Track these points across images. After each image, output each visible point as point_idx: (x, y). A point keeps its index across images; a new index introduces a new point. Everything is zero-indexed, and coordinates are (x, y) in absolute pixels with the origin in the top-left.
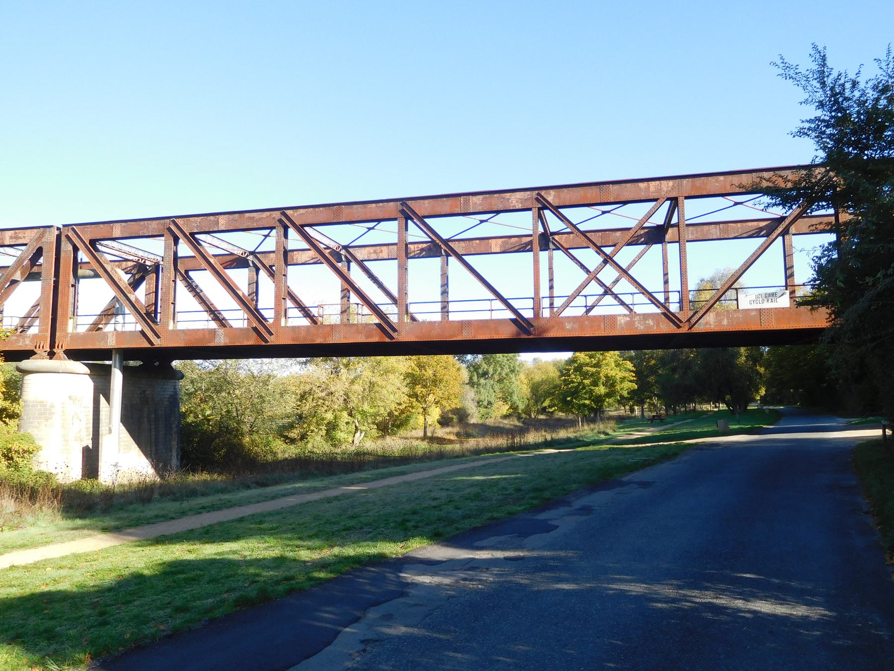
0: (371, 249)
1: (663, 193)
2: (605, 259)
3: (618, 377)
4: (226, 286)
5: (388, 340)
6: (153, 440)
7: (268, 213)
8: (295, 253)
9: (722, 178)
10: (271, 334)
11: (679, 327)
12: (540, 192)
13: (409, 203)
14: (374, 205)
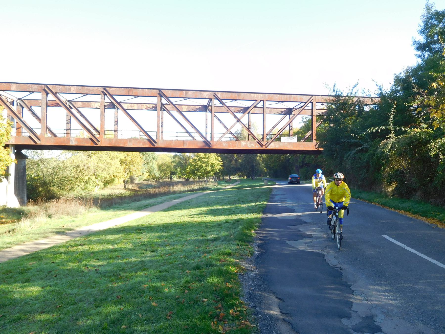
0: (129, 105)
1: (259, 98)
2: (237, 120)
3: (216, 163)
4: (76, 119)
5: (152, 146)
6: (18, 188)
7: (97, 88)
8: (91, 103)
9: (278, 95)
10: (98, 141)
11: (262, 147)
12: (215, 92)
13: (162, 91)
14: (147, 90)
